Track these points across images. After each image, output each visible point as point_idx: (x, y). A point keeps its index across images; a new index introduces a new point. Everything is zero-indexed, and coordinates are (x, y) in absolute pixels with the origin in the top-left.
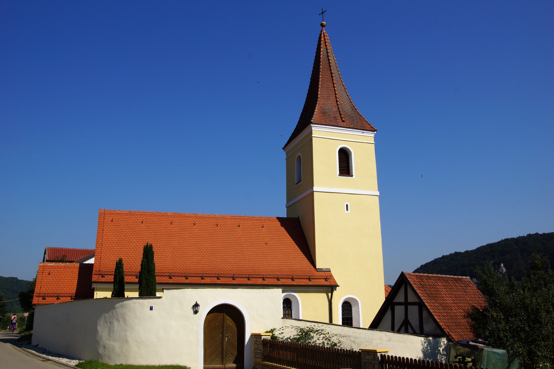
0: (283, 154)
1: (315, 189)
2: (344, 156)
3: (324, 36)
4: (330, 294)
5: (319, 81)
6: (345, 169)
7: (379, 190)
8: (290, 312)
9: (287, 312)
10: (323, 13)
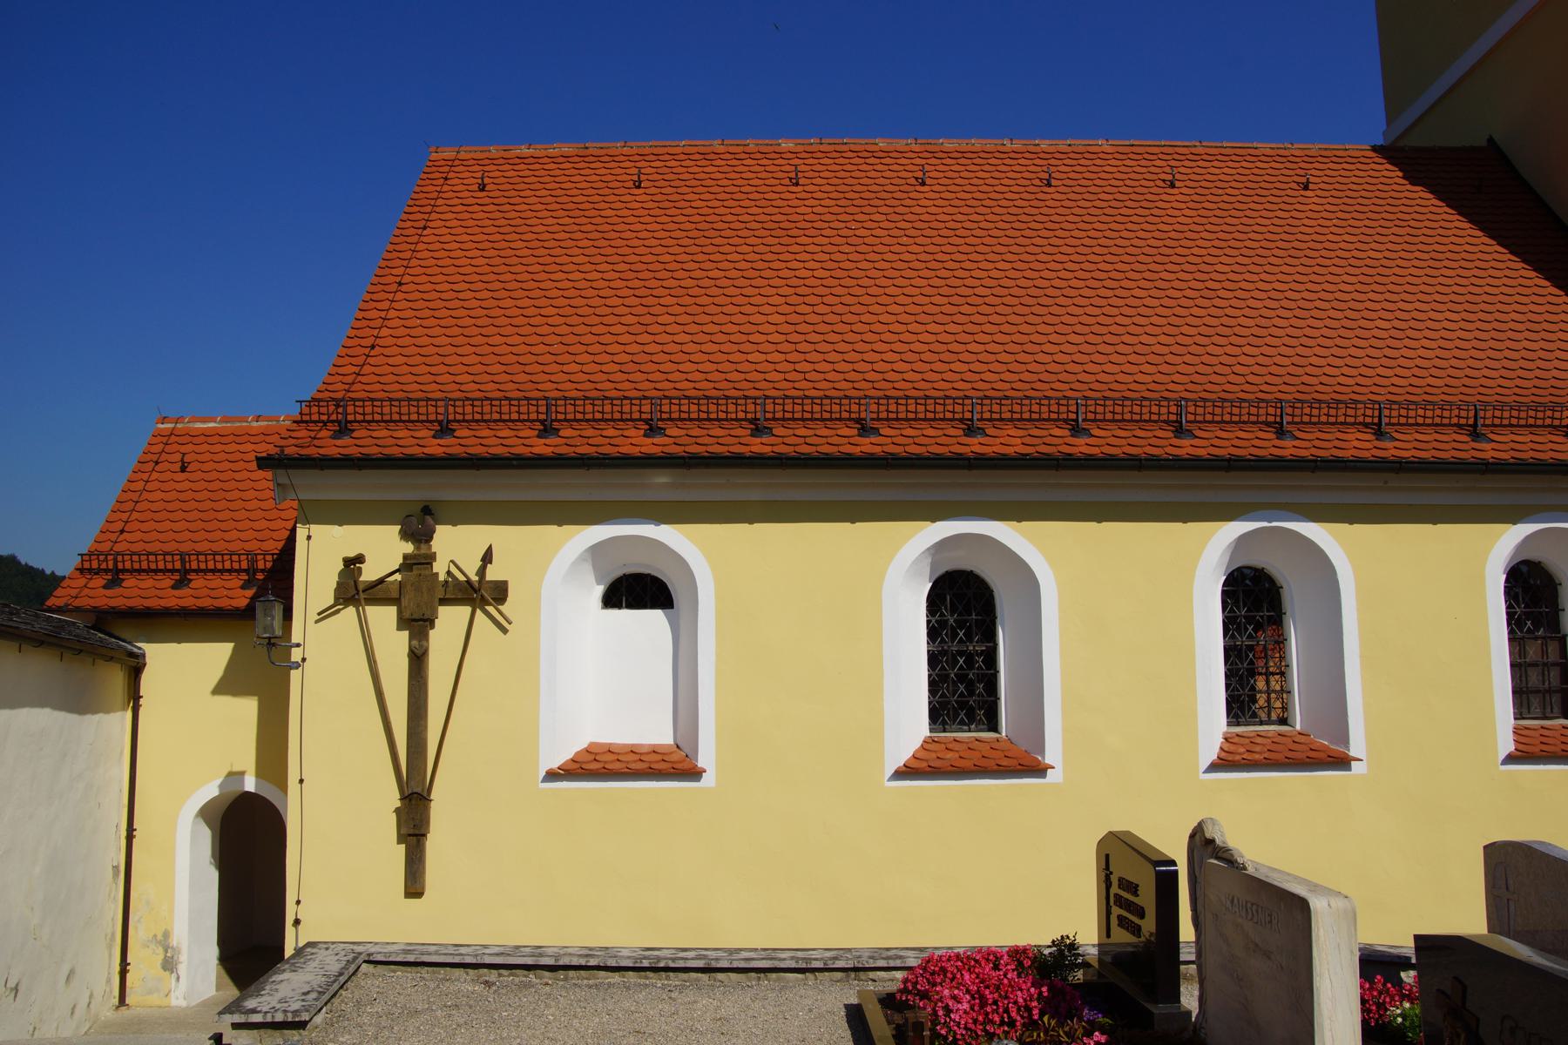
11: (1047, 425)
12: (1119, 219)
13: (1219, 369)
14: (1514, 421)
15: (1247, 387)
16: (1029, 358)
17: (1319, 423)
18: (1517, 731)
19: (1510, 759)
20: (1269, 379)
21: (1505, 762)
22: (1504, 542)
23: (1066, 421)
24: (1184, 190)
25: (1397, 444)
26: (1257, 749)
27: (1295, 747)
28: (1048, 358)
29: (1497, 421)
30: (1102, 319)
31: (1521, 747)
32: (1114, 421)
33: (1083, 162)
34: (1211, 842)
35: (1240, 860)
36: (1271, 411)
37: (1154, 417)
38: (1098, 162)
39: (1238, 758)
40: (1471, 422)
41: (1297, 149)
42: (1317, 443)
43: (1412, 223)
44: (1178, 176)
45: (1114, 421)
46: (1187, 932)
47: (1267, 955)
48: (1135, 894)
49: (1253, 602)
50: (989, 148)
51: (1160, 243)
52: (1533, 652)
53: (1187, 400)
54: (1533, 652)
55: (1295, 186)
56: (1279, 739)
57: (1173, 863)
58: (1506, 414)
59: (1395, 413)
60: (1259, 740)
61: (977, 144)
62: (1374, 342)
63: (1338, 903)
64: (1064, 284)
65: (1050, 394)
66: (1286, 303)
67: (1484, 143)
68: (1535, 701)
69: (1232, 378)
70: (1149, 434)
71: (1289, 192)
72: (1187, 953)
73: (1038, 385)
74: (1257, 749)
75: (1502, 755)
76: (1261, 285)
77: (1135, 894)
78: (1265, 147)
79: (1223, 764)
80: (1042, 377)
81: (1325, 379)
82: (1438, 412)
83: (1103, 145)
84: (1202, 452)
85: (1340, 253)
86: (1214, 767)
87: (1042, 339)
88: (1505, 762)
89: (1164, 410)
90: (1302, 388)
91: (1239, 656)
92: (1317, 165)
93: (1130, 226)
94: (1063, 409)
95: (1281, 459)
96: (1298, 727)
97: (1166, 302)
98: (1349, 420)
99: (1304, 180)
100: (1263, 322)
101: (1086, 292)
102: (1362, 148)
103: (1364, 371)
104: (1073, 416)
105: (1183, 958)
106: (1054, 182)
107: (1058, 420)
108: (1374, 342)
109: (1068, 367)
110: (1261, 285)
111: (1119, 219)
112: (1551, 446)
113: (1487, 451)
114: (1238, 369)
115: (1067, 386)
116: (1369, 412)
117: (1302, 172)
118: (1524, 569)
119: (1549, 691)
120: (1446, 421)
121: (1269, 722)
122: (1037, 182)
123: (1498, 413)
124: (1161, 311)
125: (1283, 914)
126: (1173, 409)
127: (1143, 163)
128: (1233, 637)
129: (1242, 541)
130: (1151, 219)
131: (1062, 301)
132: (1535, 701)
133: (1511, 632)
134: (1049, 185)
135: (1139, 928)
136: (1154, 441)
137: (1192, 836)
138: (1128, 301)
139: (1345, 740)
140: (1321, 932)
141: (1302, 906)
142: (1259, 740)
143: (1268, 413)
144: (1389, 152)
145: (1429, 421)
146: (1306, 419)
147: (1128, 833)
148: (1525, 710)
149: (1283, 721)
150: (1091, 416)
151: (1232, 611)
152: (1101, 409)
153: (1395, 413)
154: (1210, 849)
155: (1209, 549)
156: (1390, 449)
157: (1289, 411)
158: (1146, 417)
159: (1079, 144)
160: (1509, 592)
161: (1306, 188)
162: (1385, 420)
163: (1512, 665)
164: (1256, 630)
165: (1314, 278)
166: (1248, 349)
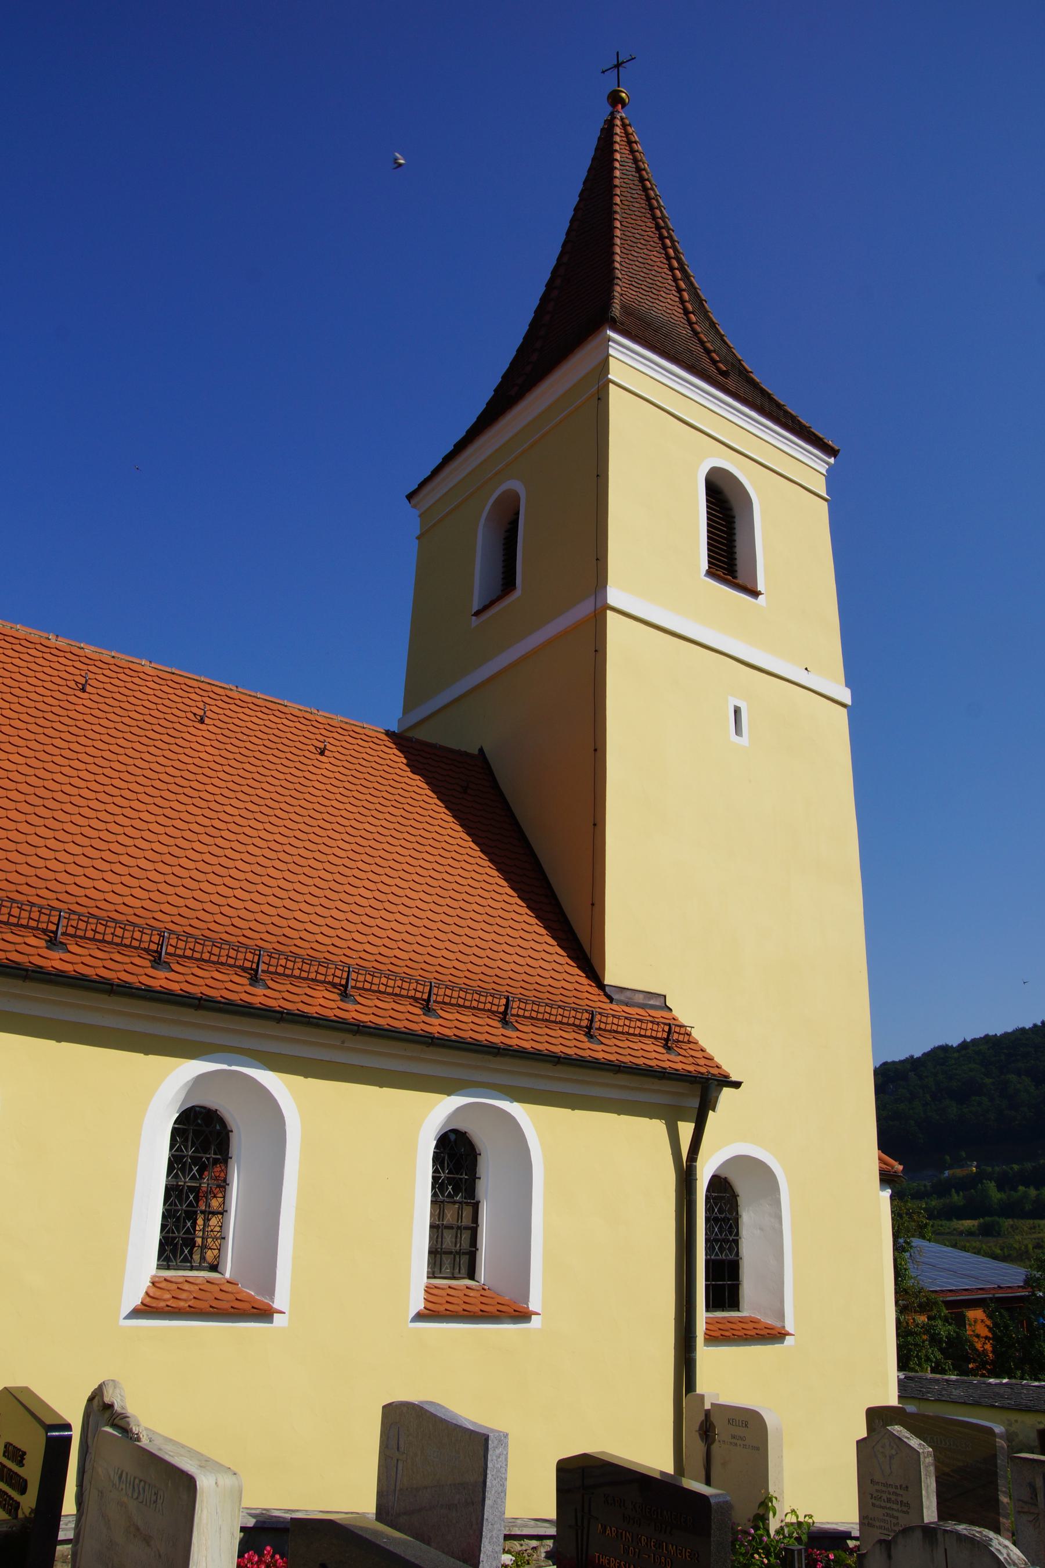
0: (409, 521)
1: (614, 596)
2: (726, 511)
3: (624, 126)
4: (686, 1130)
5: (612, 237)
6: (728, 555)
7: (850, 681)
8: (467, 1212)
9: (450, 1215)
10: (618, 66)
11: (23, 932)
12: (144, 740)
13: (209, 907)
14: (461, 1002)
15: (231, 929)
16: (21, 859)
17: (292, 976)
18: (428, 1290)
19: (420, 1317)
20: (254, 925)
21: (414, 1320)
22: (436, 1111)
23: (45, 931)
24: (212, 729)
25: (358, 1007)
26: (184, 1295)
27: (221, 1295)
28: (41, 863)
29: (447, 1000)
30: (105, 835)
31: (430, 1306)
32: (93, 939)
33: (122, 676)
34: (110, 1407)
35: (135, 1430)
36: (249, 956)
37: (135, 943)
38: (137, 680)
39: (162, 1304)
40: (425, 996)
41: (321, 716)
42: (287, 995)
43: (406, 807)
44: (209, 713)
45: (93, 939)
46: (69, 1506)
47: (147, 1540)
48: (21, 1463)
49: (202, 1141)
50: (33, 638)
51: (177, 773)
52: (450, 1216)
53: (171, 932)
54: (450, 1216)
55: (313, 749)
56: (208, 1287)
57: (68, 1427)
58: (455, 994)
59: (361, 978)
60: (186, 1286)
61: (21, 630)
62: (355, 908)
63: (226, 1481)
64: (75, 791)
65: (35, 900)
66: (282, 856)
67: (476, 752)
68: (447, 1261)
69: (219, 918)
70: (127, 960)
71: (307, 754)
72: (66, 1532)
73: (25, 889)
74: (184, 1295)
75: (412, 1313)
76: (264, 834)
77: (21, 1463)
78: (294, 707)
79: (145, 1310)
80: (30, 881)
81: (305, 935)
82: (399, 983)
83: (146, 665)
84: (175, 987)
85: (340, 820)
86: (137, 1313)
87: (39, 842)
88: (414, 1320)
89: (146, 938)
90: (283, 939)
91: (179, 1197)
92: (335, 735)
93: (152, 750)
94: (44, 918)
95: (249, 1006)
96: (228, 1275)
97: (171, 831)
98: (320, 978)
99: (322, 746)
100: (259, 869)
101: (95, 804)
102: (376, 729)
103: (341, 933)
104: (53, 927)
105: (62, 1536)
106: (88, 689)
107: (37, 929)
108: (355, 908)
109: (59, 876)
110: (264, 834)
111: (144, 740)
112: (488, 1029)
113: (435, 1026)
114: (226, 910)
115: (54, 895)
116: (338, 973)
117: (321, 738)
118: (453, 1137)
119: (459, 1253)
120: (404, 992)
121: (199, 1268)
122: (72, 684)
123: (449, 992)
124: (164, 839)
125: (169, 1490)
126: (156, 938)
127: (180, 692)
128: (176, 1176)
129: (201, 1080)
130: (174, 748)
131: (69, 808)
132: (447, 1261)
133: (434, 1195)
134: (83, 690)
135: (18, 1505)
136: (130, 968)
137: (91, 1400)
138: (179, 797)
139: (271, 1292)
140: (205, 1512)
141: (187, 1484)
142: (186, 1286)
143: (244, 958)
144: (400, 740)
145: (390, 990)
146: (280, 970)
147: (26, 1390)
148: (437, 1270)
149: (214, 1268)
150: (71, 931)
151: (179, 1149)
152: (82, 925)
153: (361, 978)
154: (107, 1415)
155: (165, 1085)
156: (351, 1012)
157: (266, 959)
158: (127, 942)
159: (123, 659)
160: (437, 1159)
161: (322, 753)
162: (351, 983)
163: (432, 1227)
164: (201, 1172)
165: (313, 837)
166: (239, 893)
